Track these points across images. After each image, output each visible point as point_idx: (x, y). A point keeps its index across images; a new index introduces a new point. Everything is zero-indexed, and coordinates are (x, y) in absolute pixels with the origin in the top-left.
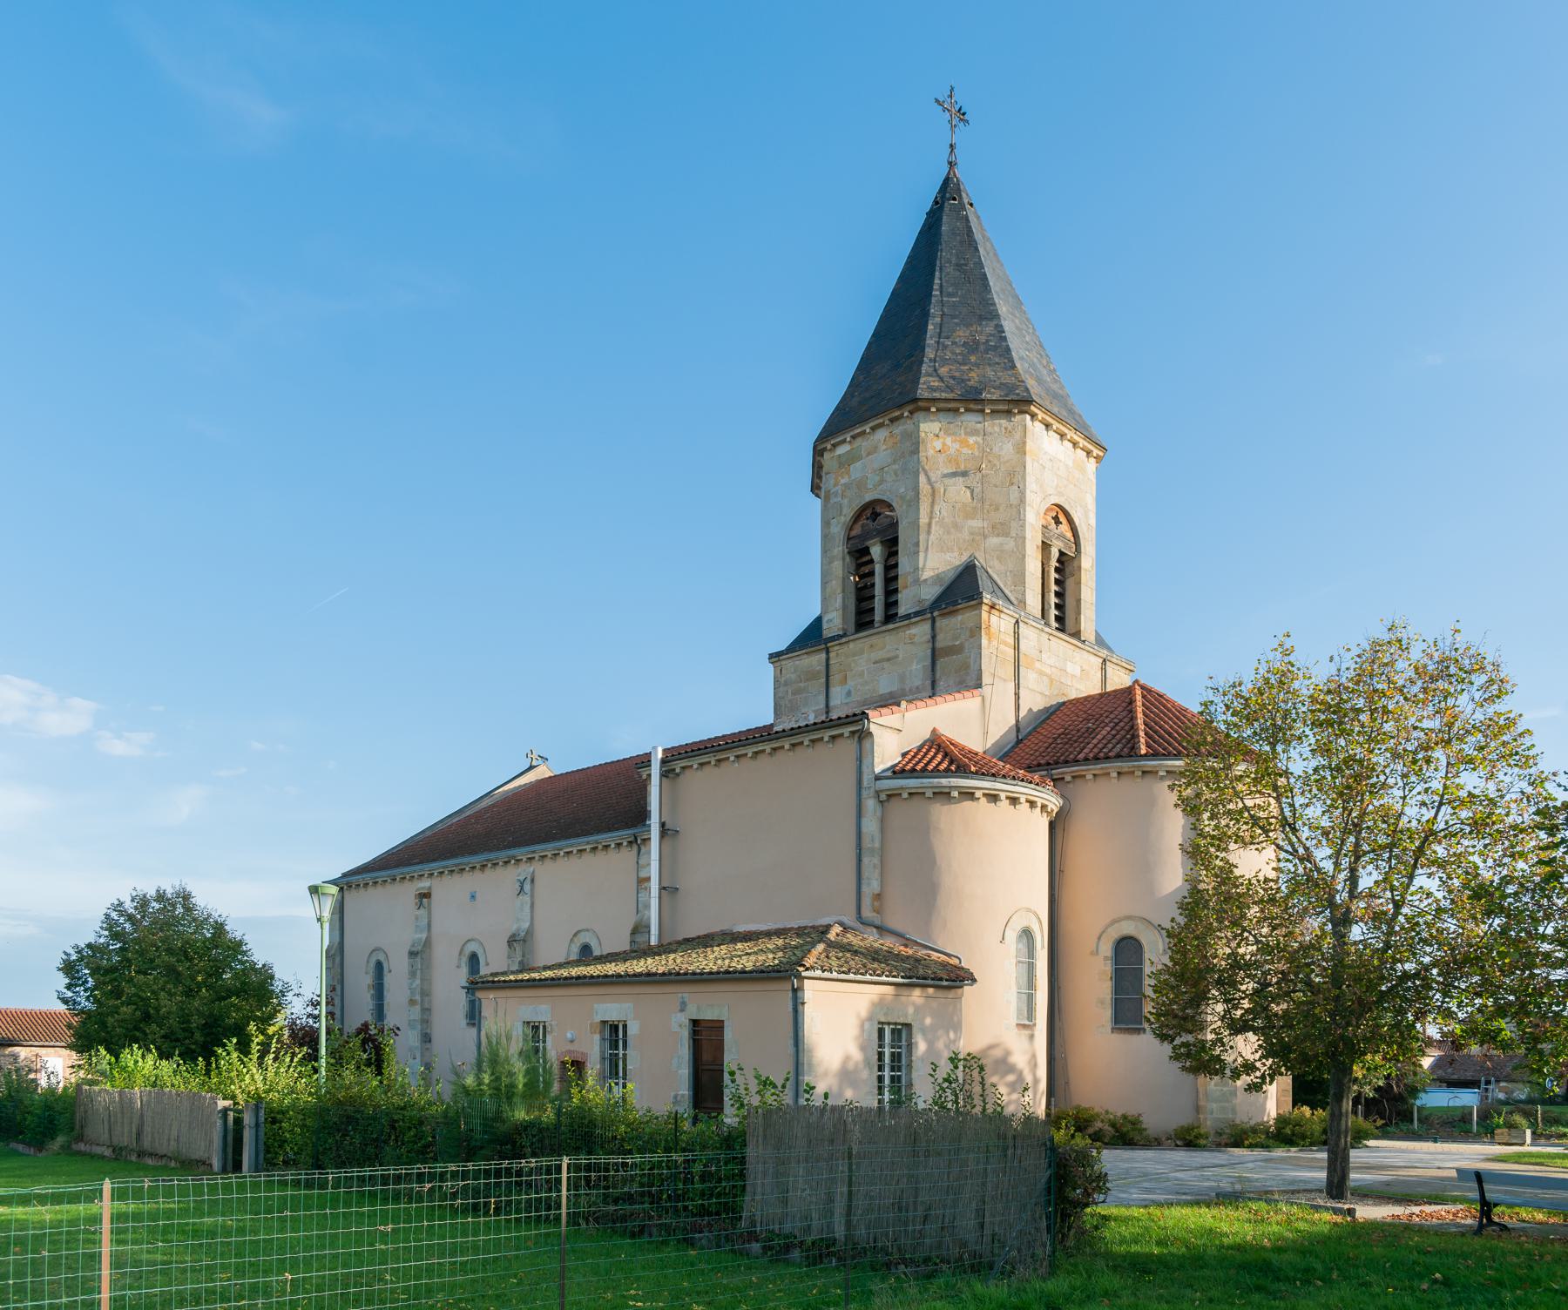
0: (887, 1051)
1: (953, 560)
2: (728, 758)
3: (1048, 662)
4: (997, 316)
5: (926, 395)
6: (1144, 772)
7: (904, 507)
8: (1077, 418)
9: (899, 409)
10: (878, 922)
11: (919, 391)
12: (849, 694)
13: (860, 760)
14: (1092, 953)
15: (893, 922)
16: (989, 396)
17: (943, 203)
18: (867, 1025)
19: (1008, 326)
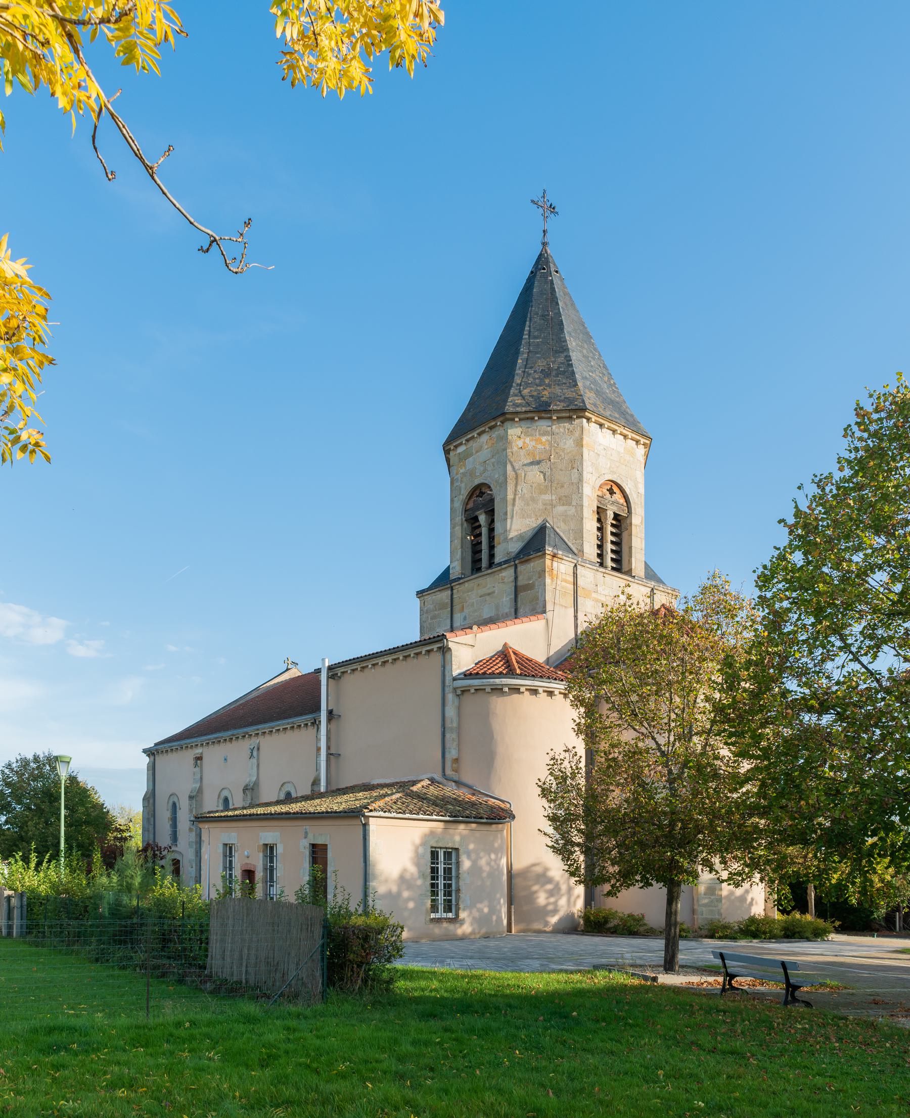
0: (441, 867)
2: (368, 666)
3: (603, 592)
4: (567, 350)
5: (511, 410)
8: (628, 417)
10: (456, 778)
11: (507, 407)
12: (465, 618)
13: (444, 667)
15: (467, 778)
16: (555, 408)
17: (536, 273)
18: (421, 850)
19: (575, 356)
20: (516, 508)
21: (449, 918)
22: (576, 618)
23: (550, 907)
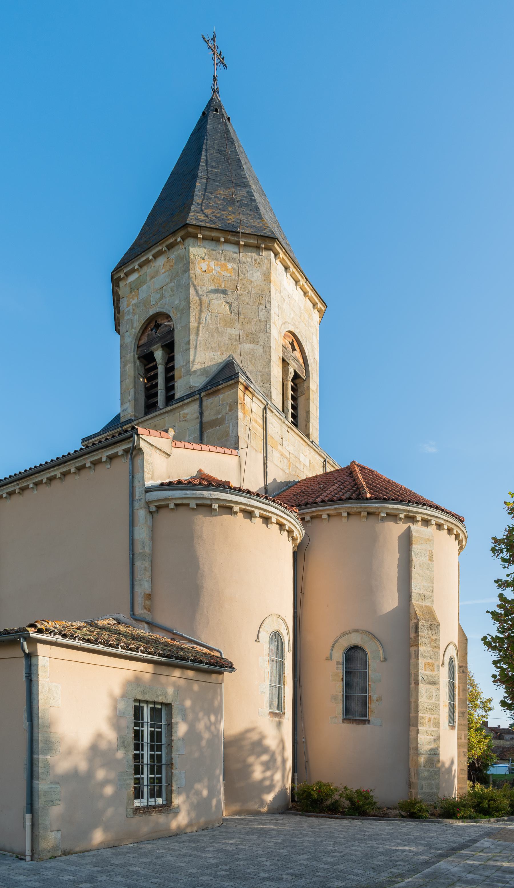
0: (146, 730)
1: (216, 358)
5: (194, 222)
6: (369, 513)
7: (179, 315)
9: (174, 236)
10: (149, 619)
14: (327, 659)
15: (162, 619)
16: (243, 231)
18: (121, 705)
20: (200, 338)
21: (159, 806)
22: (265, 465)
23: (267, 783)
